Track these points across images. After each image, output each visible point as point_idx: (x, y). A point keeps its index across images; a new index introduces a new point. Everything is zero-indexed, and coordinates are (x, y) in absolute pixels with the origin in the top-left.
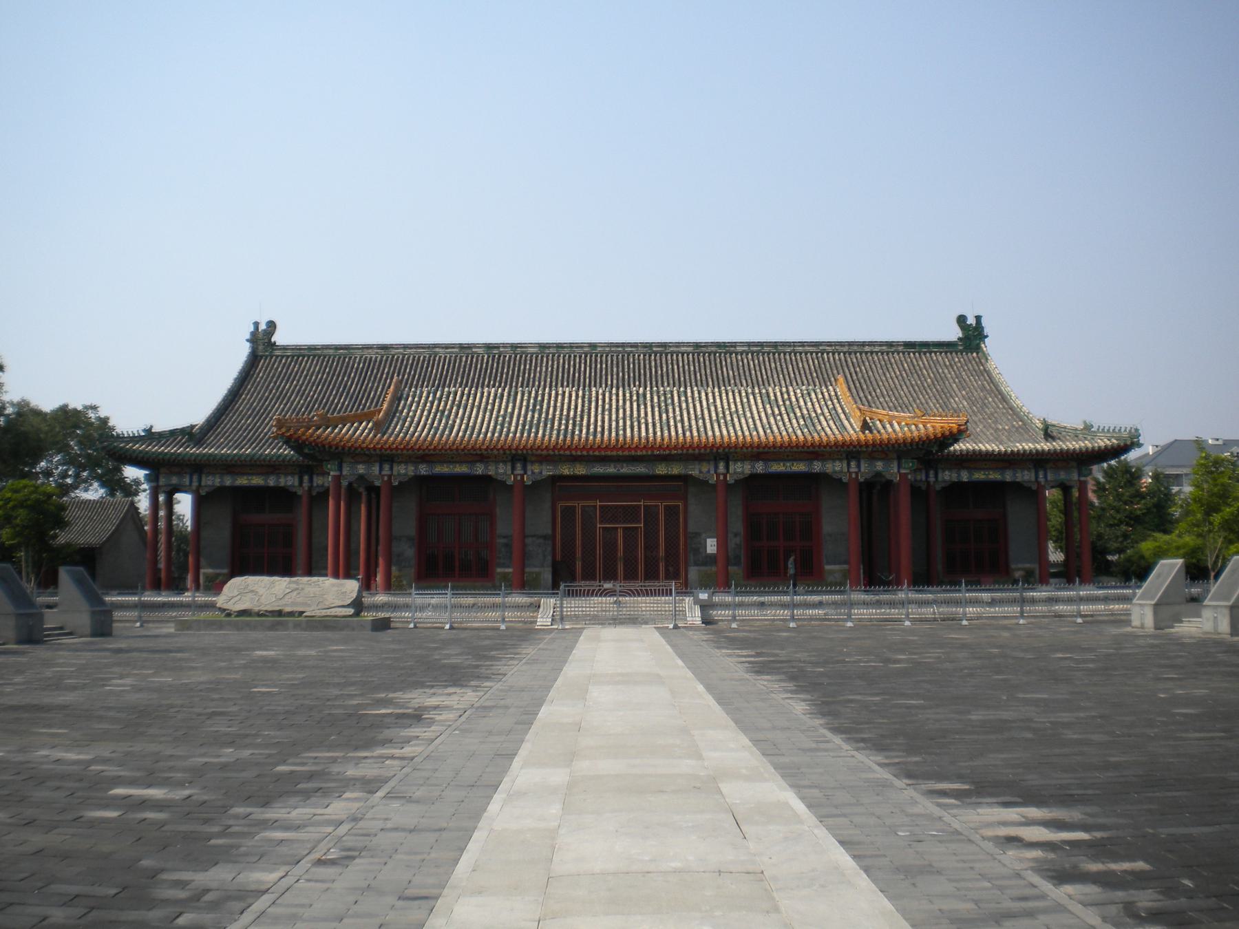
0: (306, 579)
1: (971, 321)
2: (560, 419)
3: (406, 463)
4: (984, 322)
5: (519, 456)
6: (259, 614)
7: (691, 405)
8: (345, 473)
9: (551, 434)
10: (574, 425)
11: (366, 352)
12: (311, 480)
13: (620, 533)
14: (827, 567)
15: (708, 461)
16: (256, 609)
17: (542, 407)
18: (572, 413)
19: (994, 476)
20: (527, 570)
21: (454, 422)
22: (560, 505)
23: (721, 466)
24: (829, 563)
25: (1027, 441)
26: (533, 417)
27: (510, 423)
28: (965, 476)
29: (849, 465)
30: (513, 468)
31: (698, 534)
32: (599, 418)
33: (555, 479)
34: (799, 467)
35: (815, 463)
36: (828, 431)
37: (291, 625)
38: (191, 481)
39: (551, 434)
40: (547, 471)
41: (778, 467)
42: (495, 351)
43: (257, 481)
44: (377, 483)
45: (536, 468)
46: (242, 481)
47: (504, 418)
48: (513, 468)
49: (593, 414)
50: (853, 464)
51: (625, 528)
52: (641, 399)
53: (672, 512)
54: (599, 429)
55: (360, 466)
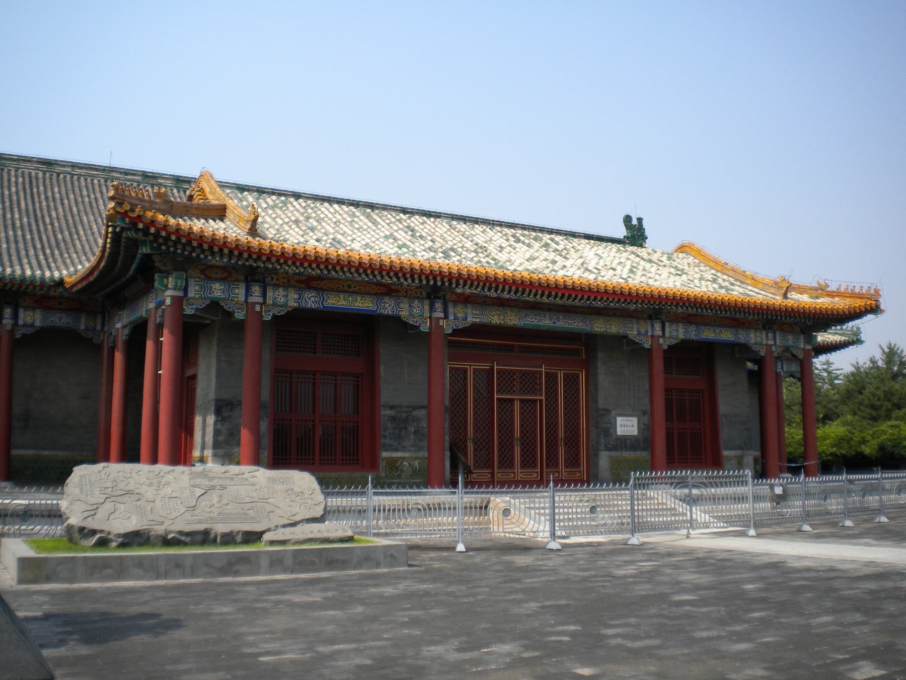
0: (263, 474)
4: (645, 225)
6: (167, 542)
8: (191, 294)
11: (23, 165)
12: (15, 316)
13: (517, 405)
14: (726, 453)
16: (160, 530)
20: (14, 452)
24: (727, 449)
30: (432, 308)
31: (607, 411)
37: (265, 562)
40: (473, 316)
44: (240, 315)
51: (522, 401)
53: (572, 382)
55: (217, 286)
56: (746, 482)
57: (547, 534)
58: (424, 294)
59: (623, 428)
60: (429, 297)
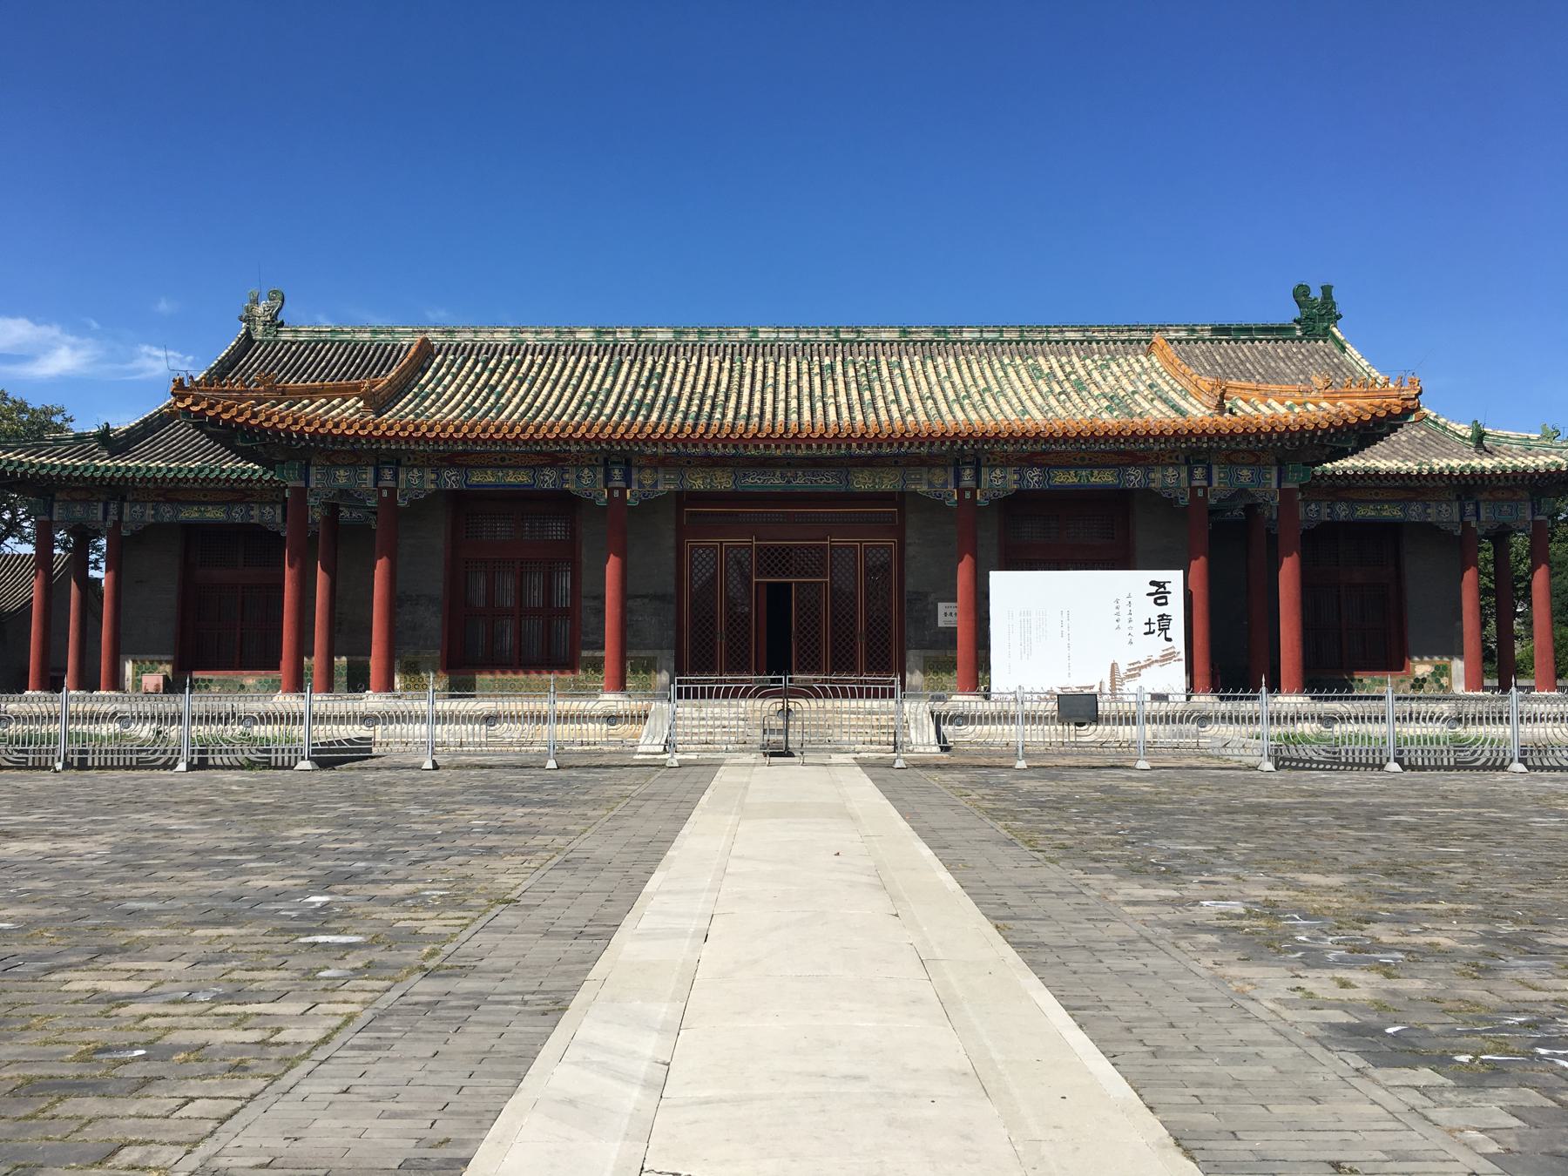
1: (1316, 294)
2: (690, 399)
3: (421, 468)
5: (617, 454)
7: (911, 381)
9: (672, 418)
10: (713, 407)
15: (944, 467)
17: (661, 382)
18: (711, 391)
19: (1391, 512)
21: (509, 401)
22: (689, 542)
23: (967, 474)
25: (1446, 456)
26: (644, 395)
27: (604, 404)
28: (1342, 512)
29: (1191, 475)
32: (757, 396)
33: (685, 499)
34: (1104, 478)
35: (1131, 470)
36: (1156, 414)
38: (106, 513)
39: (672, 418)
40: (666, 484)
41: (1065, 478)
42: (609, 338)
43: (215, 514)
45: (647, 477)
46: (191, 514)
47: (595, 395)
48: (608, 477)
49: (746, 391)
50: (1199, 472)
52: (827, 373)
54: (756, 411)
56: (892, 691)
57: (936, 749)
58: (1182, 457)
59: (949, 618)
60: (1187, 462)
